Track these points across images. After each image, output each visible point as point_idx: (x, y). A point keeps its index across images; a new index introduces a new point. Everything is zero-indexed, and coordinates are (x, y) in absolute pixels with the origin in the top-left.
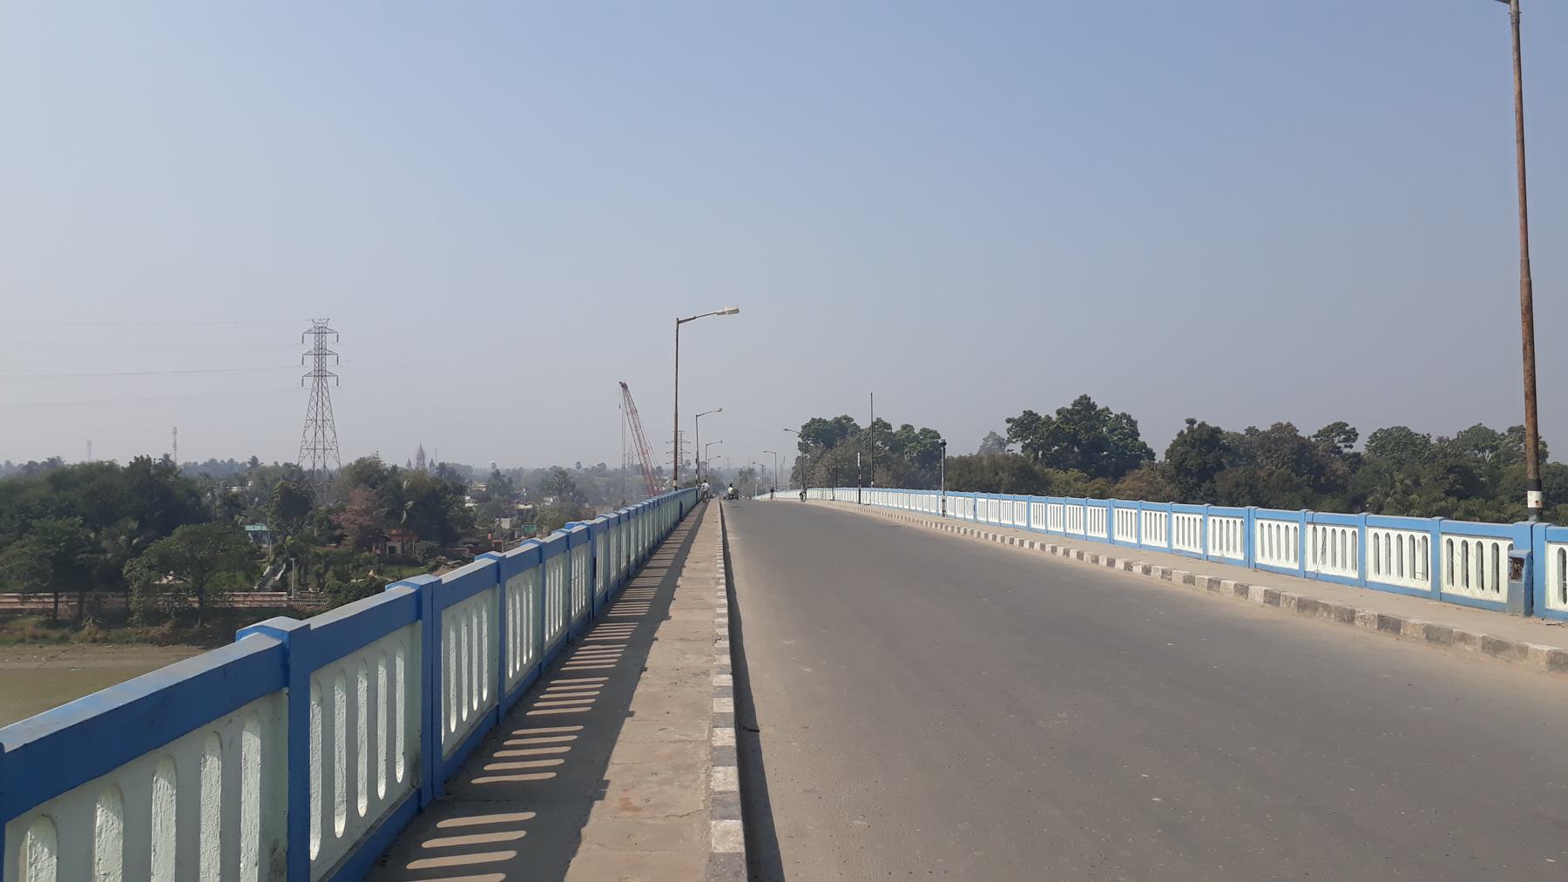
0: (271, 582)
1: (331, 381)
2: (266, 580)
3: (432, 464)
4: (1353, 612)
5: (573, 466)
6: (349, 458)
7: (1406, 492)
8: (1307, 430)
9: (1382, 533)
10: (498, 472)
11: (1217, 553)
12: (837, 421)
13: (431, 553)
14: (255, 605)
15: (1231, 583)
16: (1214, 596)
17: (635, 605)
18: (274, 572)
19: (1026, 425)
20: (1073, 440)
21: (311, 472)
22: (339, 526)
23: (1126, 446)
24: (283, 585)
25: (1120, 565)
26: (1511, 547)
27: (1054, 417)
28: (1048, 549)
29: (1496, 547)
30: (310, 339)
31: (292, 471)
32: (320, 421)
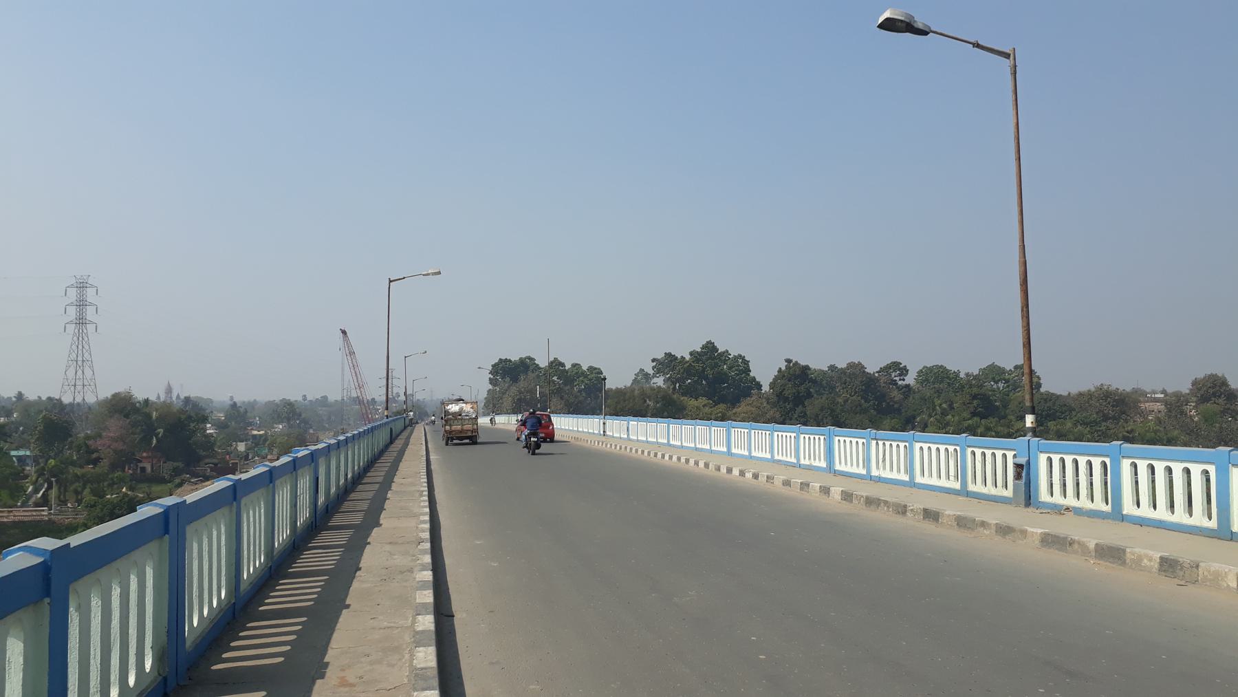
0: (33, 499)
1: (91, 328)
2: (29, 497)
3: (178, 396)
4: (905, 506)
5: (300, 399)
6: (106, 392)
7: (944, 413)
8: (872, 368)
9: (925, 446)
10: (235, 404)
11: (807, 462)
12: (522, 361)
13: (177, 472)
14: (16, 519)
15: (817, 485)
16: (805, 495)
17: (351, 515)
18: (36, 491)
19: (668, 363)
20: (702, 375)
21: (71, 405)
22: (97, 451)
23: (741, 380)
24: (45, 501)
25: (736, 472)
26: (1015, 456)
27: (688, 357)
28: (683, 460)
29: (1005, 456)
30: (73, 293)
31: (55, 405)
32: (80, 361)
